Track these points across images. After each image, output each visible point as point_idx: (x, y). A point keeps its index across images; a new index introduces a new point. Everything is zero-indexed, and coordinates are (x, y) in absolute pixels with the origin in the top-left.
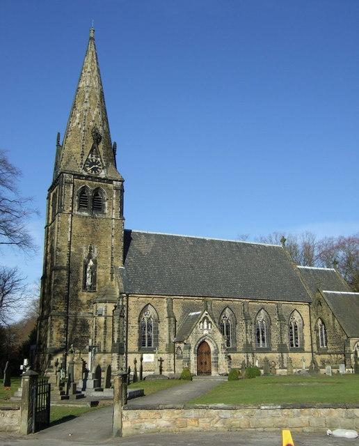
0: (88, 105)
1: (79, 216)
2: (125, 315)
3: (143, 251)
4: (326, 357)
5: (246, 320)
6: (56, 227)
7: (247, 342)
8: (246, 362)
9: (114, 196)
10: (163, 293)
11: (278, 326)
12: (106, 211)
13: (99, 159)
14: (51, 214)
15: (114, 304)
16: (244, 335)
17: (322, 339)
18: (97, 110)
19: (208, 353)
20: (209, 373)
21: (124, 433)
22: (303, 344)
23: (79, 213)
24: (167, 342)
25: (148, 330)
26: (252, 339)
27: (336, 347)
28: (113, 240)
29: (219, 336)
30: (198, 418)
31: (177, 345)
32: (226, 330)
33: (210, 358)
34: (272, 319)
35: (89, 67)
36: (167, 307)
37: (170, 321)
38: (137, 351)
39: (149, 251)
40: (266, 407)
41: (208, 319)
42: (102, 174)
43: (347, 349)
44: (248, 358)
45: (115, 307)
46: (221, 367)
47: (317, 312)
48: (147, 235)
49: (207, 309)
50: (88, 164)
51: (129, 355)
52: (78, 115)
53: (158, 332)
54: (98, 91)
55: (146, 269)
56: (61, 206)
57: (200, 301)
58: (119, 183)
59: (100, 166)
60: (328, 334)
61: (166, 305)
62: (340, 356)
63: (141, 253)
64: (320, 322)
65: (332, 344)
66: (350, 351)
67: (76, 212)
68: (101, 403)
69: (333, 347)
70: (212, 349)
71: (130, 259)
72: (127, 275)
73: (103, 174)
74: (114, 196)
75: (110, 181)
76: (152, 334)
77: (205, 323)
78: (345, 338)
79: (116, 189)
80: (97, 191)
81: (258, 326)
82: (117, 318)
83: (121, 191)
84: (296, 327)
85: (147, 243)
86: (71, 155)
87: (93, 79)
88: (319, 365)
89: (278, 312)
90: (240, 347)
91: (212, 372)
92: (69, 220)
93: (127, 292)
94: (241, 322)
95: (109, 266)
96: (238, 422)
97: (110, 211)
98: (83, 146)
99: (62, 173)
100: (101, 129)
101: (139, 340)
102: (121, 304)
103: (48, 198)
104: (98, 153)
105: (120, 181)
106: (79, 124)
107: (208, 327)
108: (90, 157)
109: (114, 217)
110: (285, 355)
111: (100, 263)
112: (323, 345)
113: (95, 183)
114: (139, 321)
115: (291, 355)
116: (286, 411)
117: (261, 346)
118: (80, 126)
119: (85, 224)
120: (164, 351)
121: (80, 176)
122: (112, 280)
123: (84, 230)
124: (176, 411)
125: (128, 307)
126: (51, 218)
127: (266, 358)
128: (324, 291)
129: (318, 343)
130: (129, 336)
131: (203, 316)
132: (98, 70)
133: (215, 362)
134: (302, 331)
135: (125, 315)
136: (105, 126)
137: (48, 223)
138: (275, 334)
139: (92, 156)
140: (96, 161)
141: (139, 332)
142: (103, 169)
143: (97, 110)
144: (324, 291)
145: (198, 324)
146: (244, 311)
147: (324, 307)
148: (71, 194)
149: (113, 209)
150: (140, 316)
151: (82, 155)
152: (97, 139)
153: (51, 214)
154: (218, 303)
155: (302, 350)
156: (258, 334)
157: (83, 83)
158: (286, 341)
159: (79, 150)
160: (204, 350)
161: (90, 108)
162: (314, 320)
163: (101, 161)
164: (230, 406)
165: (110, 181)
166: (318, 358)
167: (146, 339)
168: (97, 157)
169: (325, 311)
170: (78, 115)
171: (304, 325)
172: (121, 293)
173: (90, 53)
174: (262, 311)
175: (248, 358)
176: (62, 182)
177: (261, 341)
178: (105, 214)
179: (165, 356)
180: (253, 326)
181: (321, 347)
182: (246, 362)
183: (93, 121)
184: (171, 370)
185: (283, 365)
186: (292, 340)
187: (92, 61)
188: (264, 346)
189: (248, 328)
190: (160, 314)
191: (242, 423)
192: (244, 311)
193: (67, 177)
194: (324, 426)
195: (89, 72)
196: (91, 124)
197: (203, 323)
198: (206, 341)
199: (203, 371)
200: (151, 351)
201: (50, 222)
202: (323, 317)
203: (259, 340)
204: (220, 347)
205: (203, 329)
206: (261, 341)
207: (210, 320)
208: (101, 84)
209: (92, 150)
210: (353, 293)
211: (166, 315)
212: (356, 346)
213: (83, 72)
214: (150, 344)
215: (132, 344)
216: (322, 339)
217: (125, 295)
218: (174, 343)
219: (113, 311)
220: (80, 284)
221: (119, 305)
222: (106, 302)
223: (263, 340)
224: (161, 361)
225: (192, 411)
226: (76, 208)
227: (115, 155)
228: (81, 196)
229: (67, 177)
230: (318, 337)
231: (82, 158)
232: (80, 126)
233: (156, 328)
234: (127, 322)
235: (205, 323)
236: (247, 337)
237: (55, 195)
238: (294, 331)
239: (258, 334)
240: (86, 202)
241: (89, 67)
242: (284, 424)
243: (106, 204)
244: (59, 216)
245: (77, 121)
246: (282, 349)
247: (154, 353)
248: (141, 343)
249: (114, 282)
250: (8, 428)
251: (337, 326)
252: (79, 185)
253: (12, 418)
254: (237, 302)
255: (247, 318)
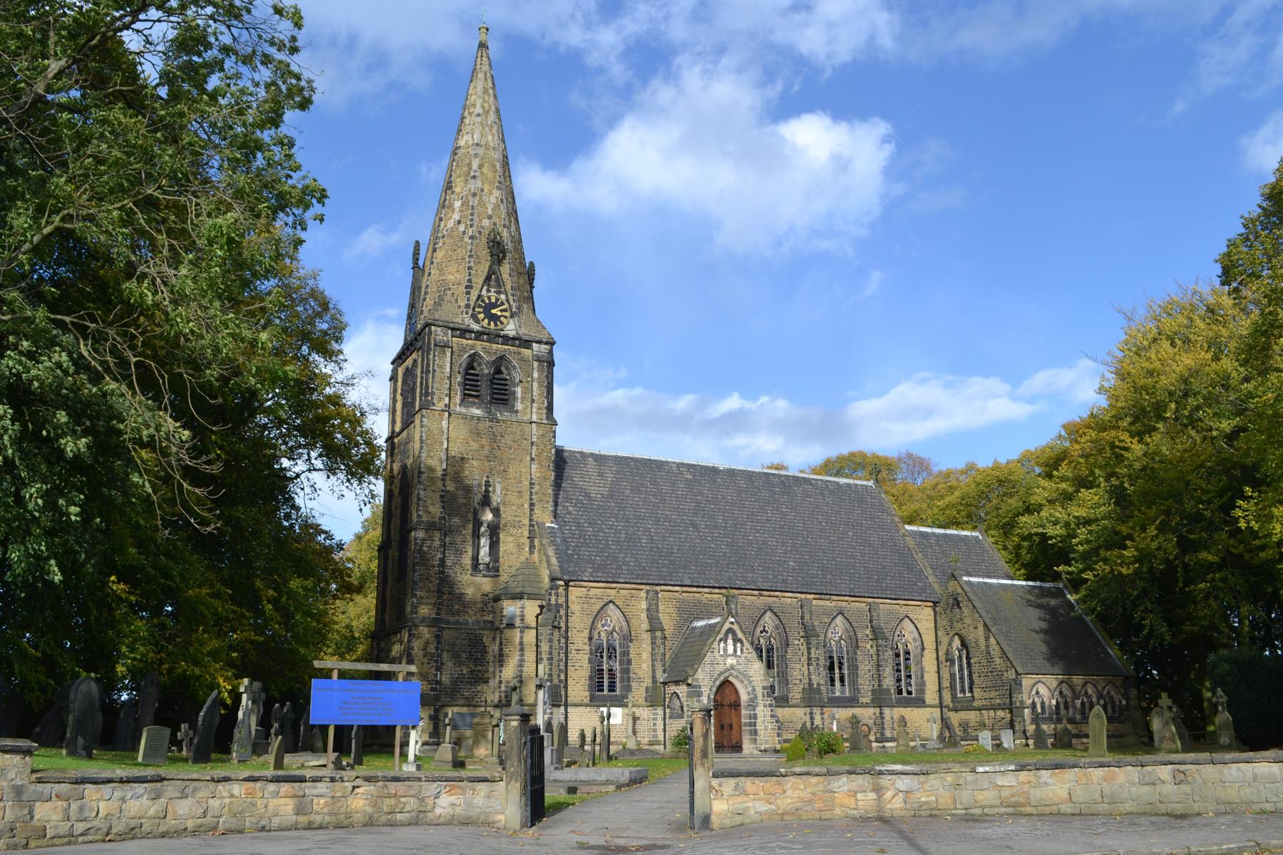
0: (479, 184)
1: (464, 417)
2: (563, 625)
3: (593, 491)
4: (972, 716)
5: (806, 637)
6: (417, 438)
7: (810, 684)
8: (808, 725)
9: (536, 375)
10: (640, 579)
11: (873, 651)
12: (519, 406)
13: (503, 297)
14: (399, 413)
15: (539, 602)
16: (805, 669)
17: (962, 678)
18: (497, 193)
19: (736, 705)
20: (737, 748)
21: (715, 820)
22: (921, 689)
23: (464, 410)
24: (648, 682)
25: (610, 657)
26: (819, 679)
27: (993, 694)
28: (534, 466)
29: (757, 669)
30: (856, 793)
31: (672, 688)
32: (768, 657)
33: (739, 716)
34: (859, 635)
35: (478, 105)
36: (648, 610)
37: (653, 638)
38: (587, 700)
39: (606, 491)
40: (987, 769)
41: (734, 634)
42: (508, 328)
43: (1017, 698)
44: (812, 718)
45: (541, 607)
46: (761, 737)
47: (951, 621)
48: (600, 459)
49: (730, 614)
50: (480, 306)
51: (569, 709)
52: (457, 204)
53: (629, 662)
54: (497, 155)
55: (601, 530)
56: (427, 394)
57: (718, 597)
58: (545, 348)
59: (505, 310)
60: (975, 668)
61: (644, 605)
62: (1000, 713)
63: (587, 495)
64: (957, 642)
65: (984, 689)
66: (1022, 702)
67: (458, 409)
68: (582, 789)
69: (986, 695)
70: (744, 697)
71: (567, 507)
72: (565, 540)
73: (510, 328)
74: (536, 375)
75: (526, 344)
76: (617, 667)
77: (730, 642)
78: (1011, 675)
79: (539, 360)
80: (500, 363)
81: (831, 651)
82: (545, 631)
83: (548, 363)
84: (908, 653)
85: (601, 475)
86: (444, 288)
87: (487, 129)
88: (958, 732)
89: (871, 621)
90: (796, 694)
91: (744, 746)
92: (445, 424)
93: (566, 578)
94: (798, 642)
95: (526, 522)
96: (933, 798)
97: (526, 407)
98: (470, 268)
99: (428, 325)
100: (505, 234)
101: (591, 678)
102: (553, 602)
103: (393, 378)
104: (499, 284)
105: (546, 343)
106: (459, 222)
107: (735, 651)
108: (484, 292)
109: (535, 418)
110: (887, 711)
111: (506, 515)
112: (963, 691)
113: (494, 346)
114: (590, 639)
115: (898, 712)
116: (1024, 776)
117: (838, 694)
118: (462, 228)
119: (476, 433)
120: (642, 701)
121: (464, 332)
122: (531, 552)
123: (475, 446)
124: (814, 780)
125: (568, 607)
126: (398, 419)
127: (854, 716)
128: (965, 579)
129: (953, 687)
130: (570, 670)
131: (727, 626)
132: (498, 110)
133: (750, 724)
134: (919, 662)
135: (563, 625)
136: (513, 229)
137: (393, 431)
138: (865, 668)
139: (488, 291)
140: (497, 300)
141: (590, 661)
142: (512, 316)
143: (497, 193)
144: (965, 579)
145: (716, 643)
146: (802, 618)
147: (966, 611)
148: (448, 369)
149: (533, 401)
150: (592, 628)
151: (469, 287)
152: (497, 250)
153: (399, 413)
154: (749, 600)
155: (920, 702)
156: (831, 668)
157: (465, 137)
158: (889, 682)
159: (462, 277)
160: (730, 698)
161: (482, 190)
162: (944, 640)
163: (508, 301)
164: (926, 768)
165: (526, 344)
166: (955, 718)
167: (606, 676)
168: (498, 292)
169: (968, 621)
170: (457, 204)
171: (923, 649)
172: (553, 579)
173: (481, 75)
174: (839, 619)
175: (812, 718)
176: (429, 343)
177: (837, 683)
178: (517, 411)
179: (644, 713)
180: (821, 651)
181: (959, 695)
182: (808, 725)
183: (490, 217)
184: (658, 743)
185: (882, 734)
186: (899, 680)
187: (485, 91)
188: (843, 692)
189: (813, 655)
190: (634, 623)
191: (941, 800)
192: (802, 618)
193: (439, 334)
194: (1100, 800)
195: (478, 115)
196: (486, 222)
197: (726, 642)
198: (730, 679)
199: (725, 743)
200: (620, 702)
201: (397, 429)
202: (963, 632)
203: (832, 680)
204: (759, 692)
205: (726, 655)
206: (837, 683)
207: (740, 635)
208: (503, 141)
209: (488, 279)
210: (1009, 582)
211: (645, 626)
212: (1034, 692)
213: (466, 114)
214: (612, 687)
215: (578, 687)
216: (962, 678)
217: (561, 583)
218: (665, 684)
219: (537, 617)
220: (467, 560)
221: (549, 604)
222: (522, 598)
223: (842, 680)
224: (635, 719)
225: (844, 779)
226: (458, 399)
227: (532, 287)
228: (467, 374)
229: (439, 334)
230: (952, 676)
231: (468, 293)
232: (462, 228)
233: (626, 653)
234: (567, 639)
235: (730, 642)
236: (809, 674)
237: (409, 373)
238: (903, 660)
239: (831, 668)
240: (475, 387)
241: (478, 105)
242: (1022, 800)
243: (519, 390)
244: (422, 416)
245: (456, 216)
246: (880, 700)
247: (624, 705)
248: (596, 683)
249: (536, 556)
250: (482, 817)
251: (995, 651)
252: (463, 350)
253: (489, 797)
254: (789, 600)
255: (809, 634)
